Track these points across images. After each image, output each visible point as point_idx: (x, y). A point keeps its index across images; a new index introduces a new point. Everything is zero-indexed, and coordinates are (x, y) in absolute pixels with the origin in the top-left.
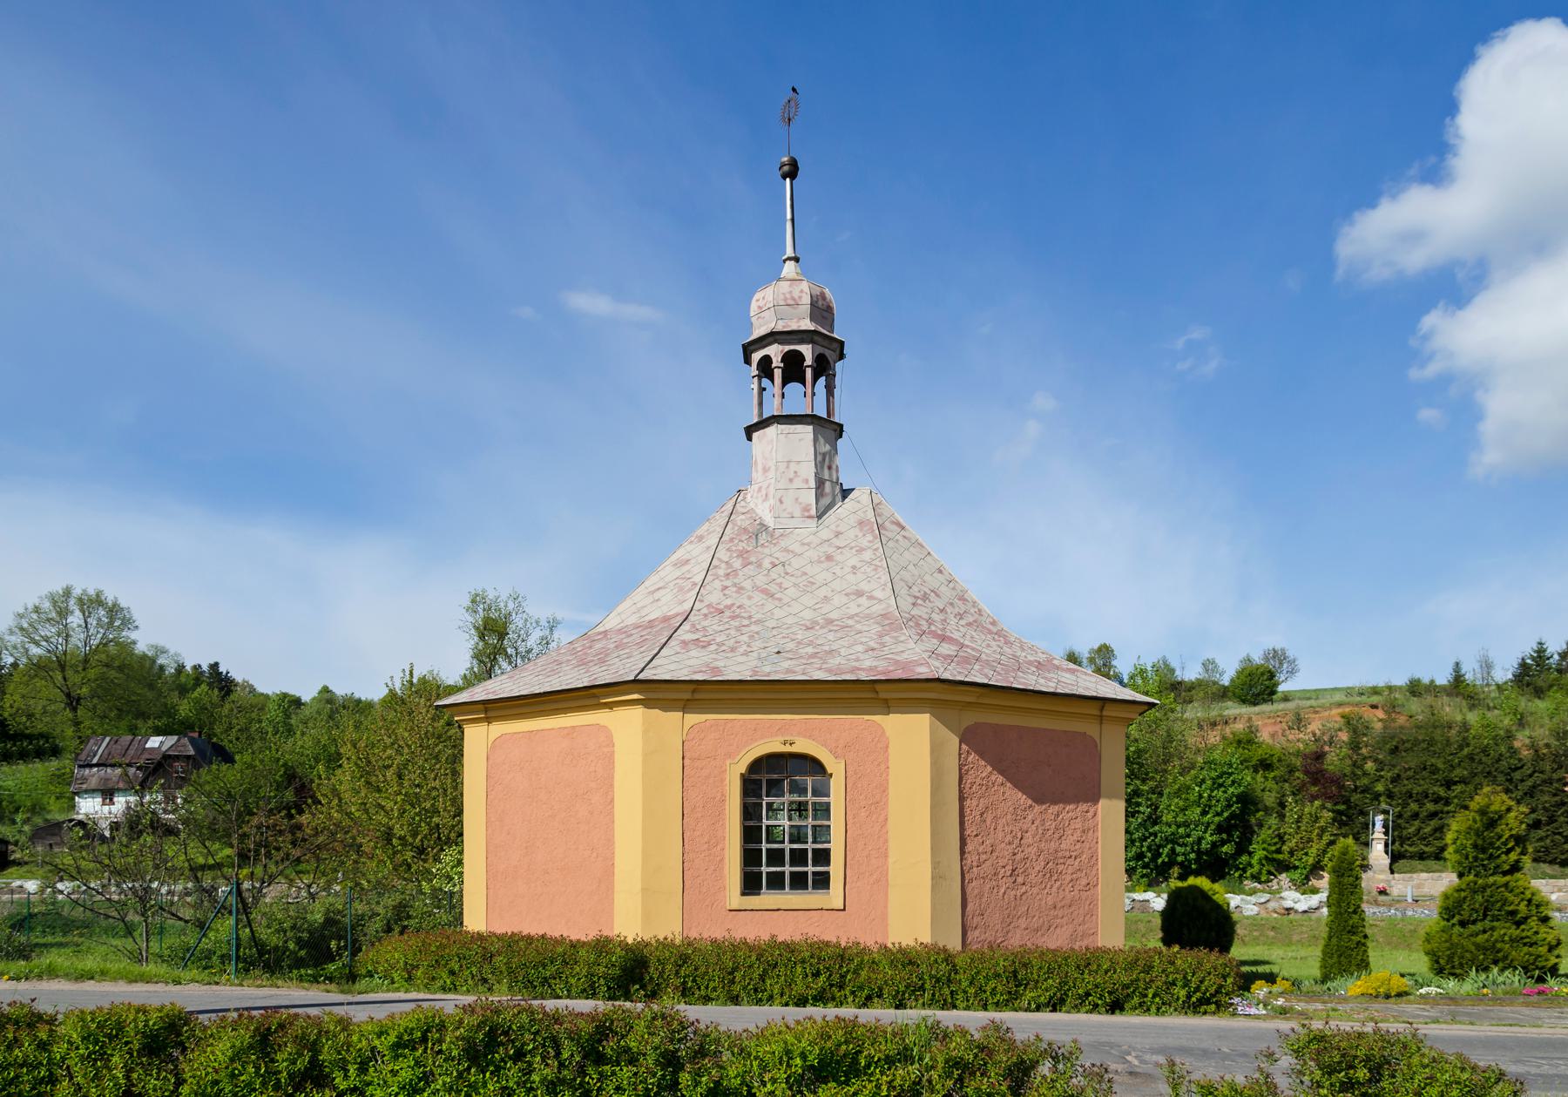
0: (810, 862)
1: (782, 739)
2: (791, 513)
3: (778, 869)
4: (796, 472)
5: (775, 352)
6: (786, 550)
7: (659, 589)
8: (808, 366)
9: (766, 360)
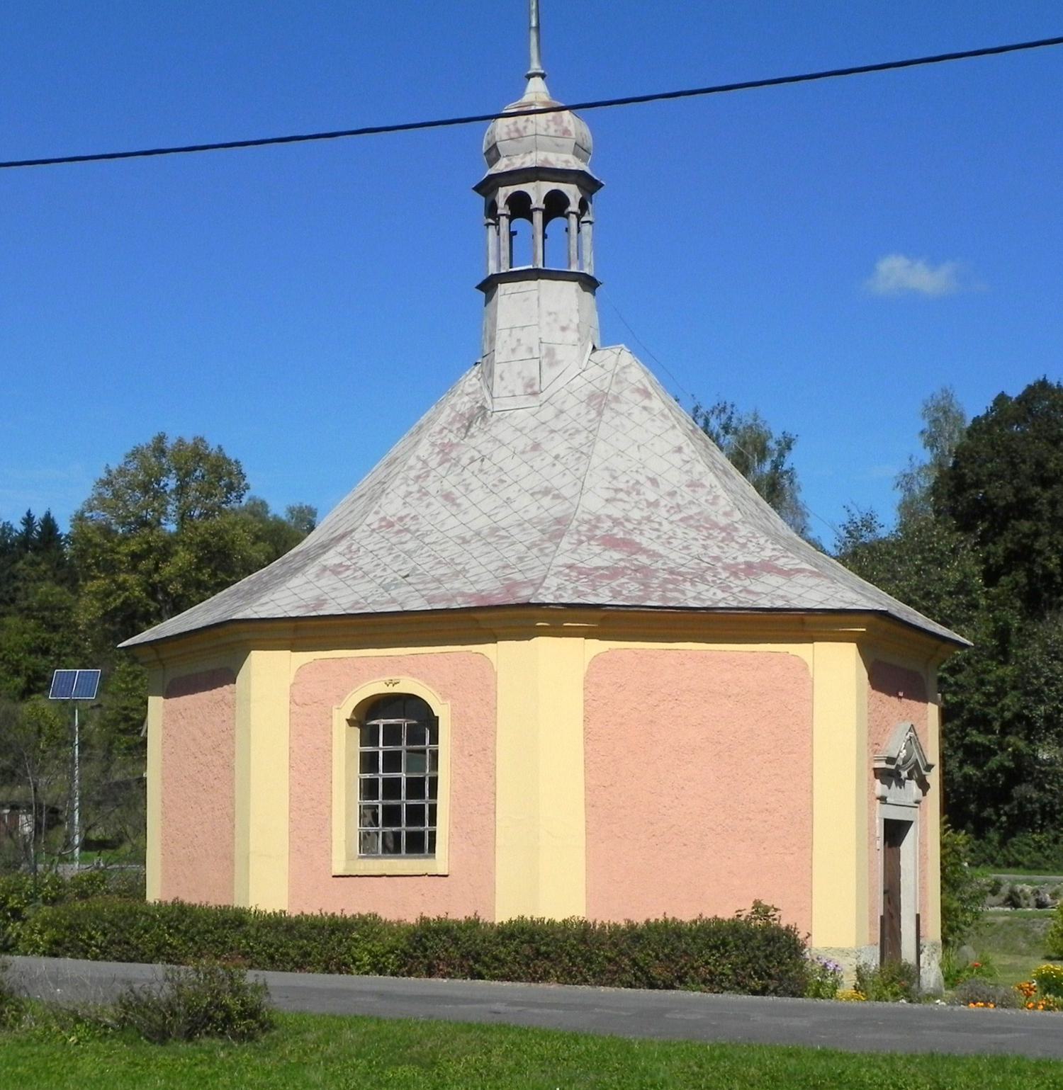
1: (387, 679)
2: (513, 391)
4: (519, 340)
5: (537, 192)
6: (495, 439)
8: (536, 209)
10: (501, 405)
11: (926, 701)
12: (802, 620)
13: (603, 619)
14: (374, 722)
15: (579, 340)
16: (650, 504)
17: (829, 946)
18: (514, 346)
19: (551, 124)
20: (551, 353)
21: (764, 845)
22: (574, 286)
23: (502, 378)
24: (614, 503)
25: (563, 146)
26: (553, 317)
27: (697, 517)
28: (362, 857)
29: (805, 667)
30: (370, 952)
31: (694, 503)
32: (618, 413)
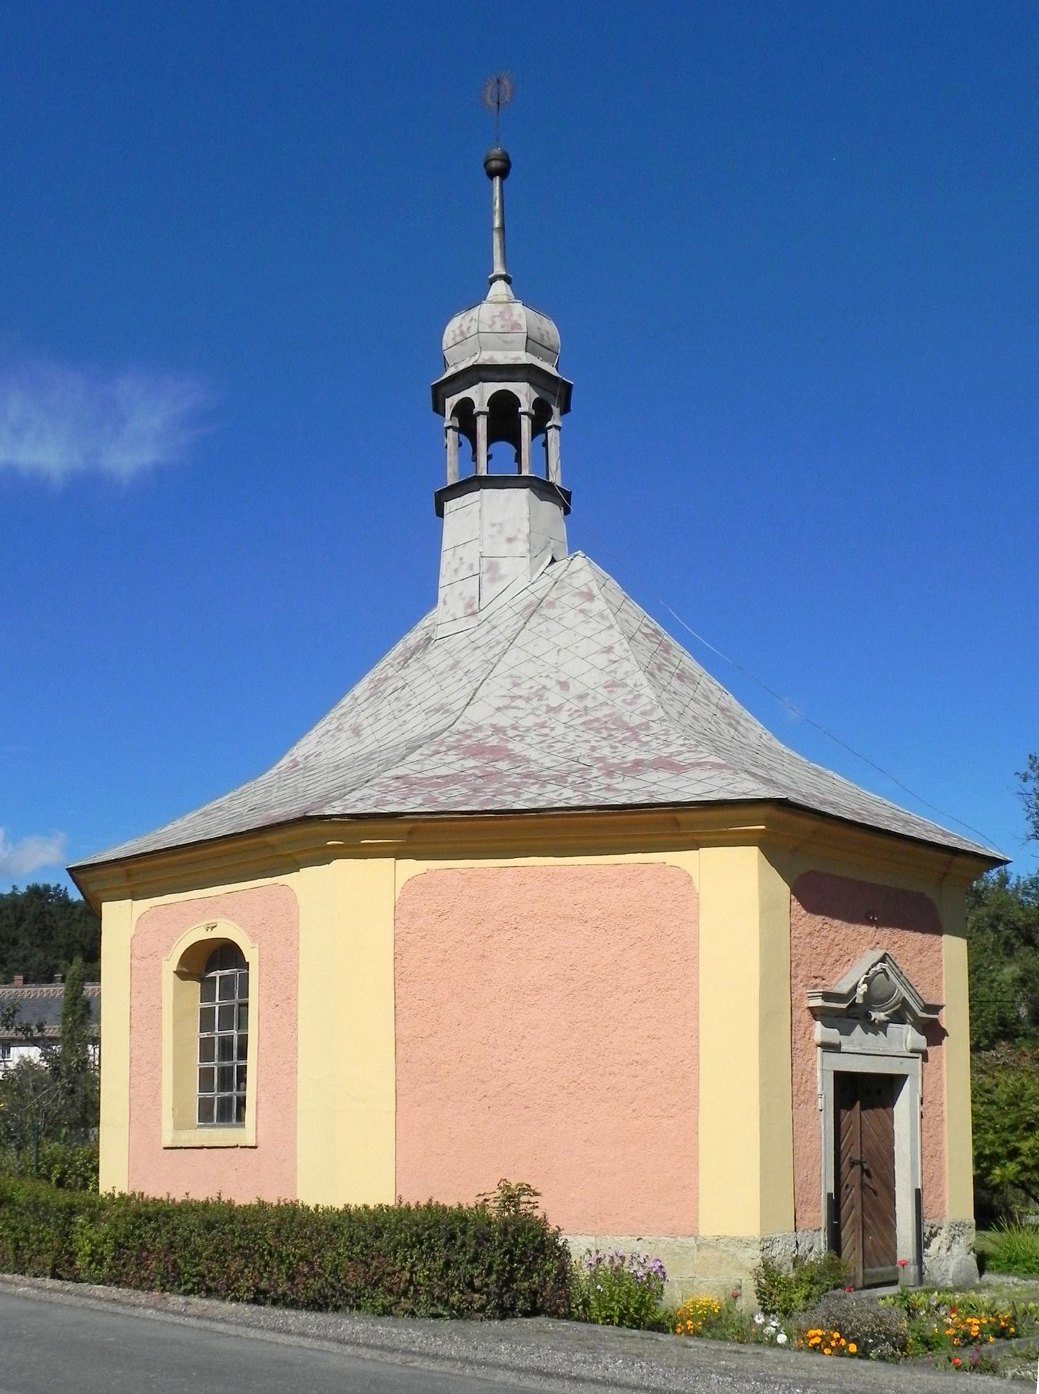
0: (216, 1040)
2: (454, 614)
3: (235, 1052)
5: (481, 394)
7: (699, 765)
8: (480, 413)
9: (467, 404)
10: (443, 631)
11: (938, 930)
12: (675, 819)
13: (410, 833)
14: (212, 974)
15: (530, 551)
16: (550, 709)
17: (722, 1234)
18: (456, 567)
19: (497, 319)
20: (493, 568)
21: (634, 1106)
22: (525, 492)
23: (445, 603)
24: (505, 712)
25: (512, 342)
26: (497, 528)
27: (604, 719)
28: (200, 1127)
29: (689, 881)
30: (91, 1241)
31: (607, 704)
32: (547, 619)
